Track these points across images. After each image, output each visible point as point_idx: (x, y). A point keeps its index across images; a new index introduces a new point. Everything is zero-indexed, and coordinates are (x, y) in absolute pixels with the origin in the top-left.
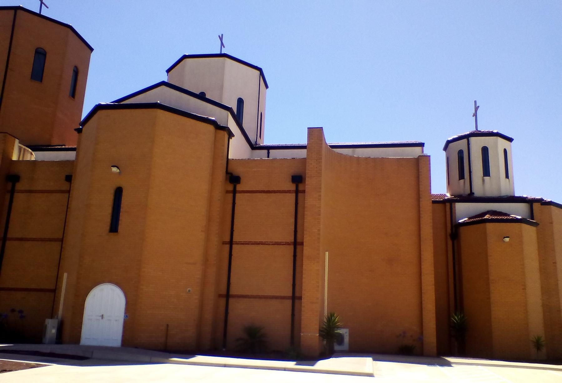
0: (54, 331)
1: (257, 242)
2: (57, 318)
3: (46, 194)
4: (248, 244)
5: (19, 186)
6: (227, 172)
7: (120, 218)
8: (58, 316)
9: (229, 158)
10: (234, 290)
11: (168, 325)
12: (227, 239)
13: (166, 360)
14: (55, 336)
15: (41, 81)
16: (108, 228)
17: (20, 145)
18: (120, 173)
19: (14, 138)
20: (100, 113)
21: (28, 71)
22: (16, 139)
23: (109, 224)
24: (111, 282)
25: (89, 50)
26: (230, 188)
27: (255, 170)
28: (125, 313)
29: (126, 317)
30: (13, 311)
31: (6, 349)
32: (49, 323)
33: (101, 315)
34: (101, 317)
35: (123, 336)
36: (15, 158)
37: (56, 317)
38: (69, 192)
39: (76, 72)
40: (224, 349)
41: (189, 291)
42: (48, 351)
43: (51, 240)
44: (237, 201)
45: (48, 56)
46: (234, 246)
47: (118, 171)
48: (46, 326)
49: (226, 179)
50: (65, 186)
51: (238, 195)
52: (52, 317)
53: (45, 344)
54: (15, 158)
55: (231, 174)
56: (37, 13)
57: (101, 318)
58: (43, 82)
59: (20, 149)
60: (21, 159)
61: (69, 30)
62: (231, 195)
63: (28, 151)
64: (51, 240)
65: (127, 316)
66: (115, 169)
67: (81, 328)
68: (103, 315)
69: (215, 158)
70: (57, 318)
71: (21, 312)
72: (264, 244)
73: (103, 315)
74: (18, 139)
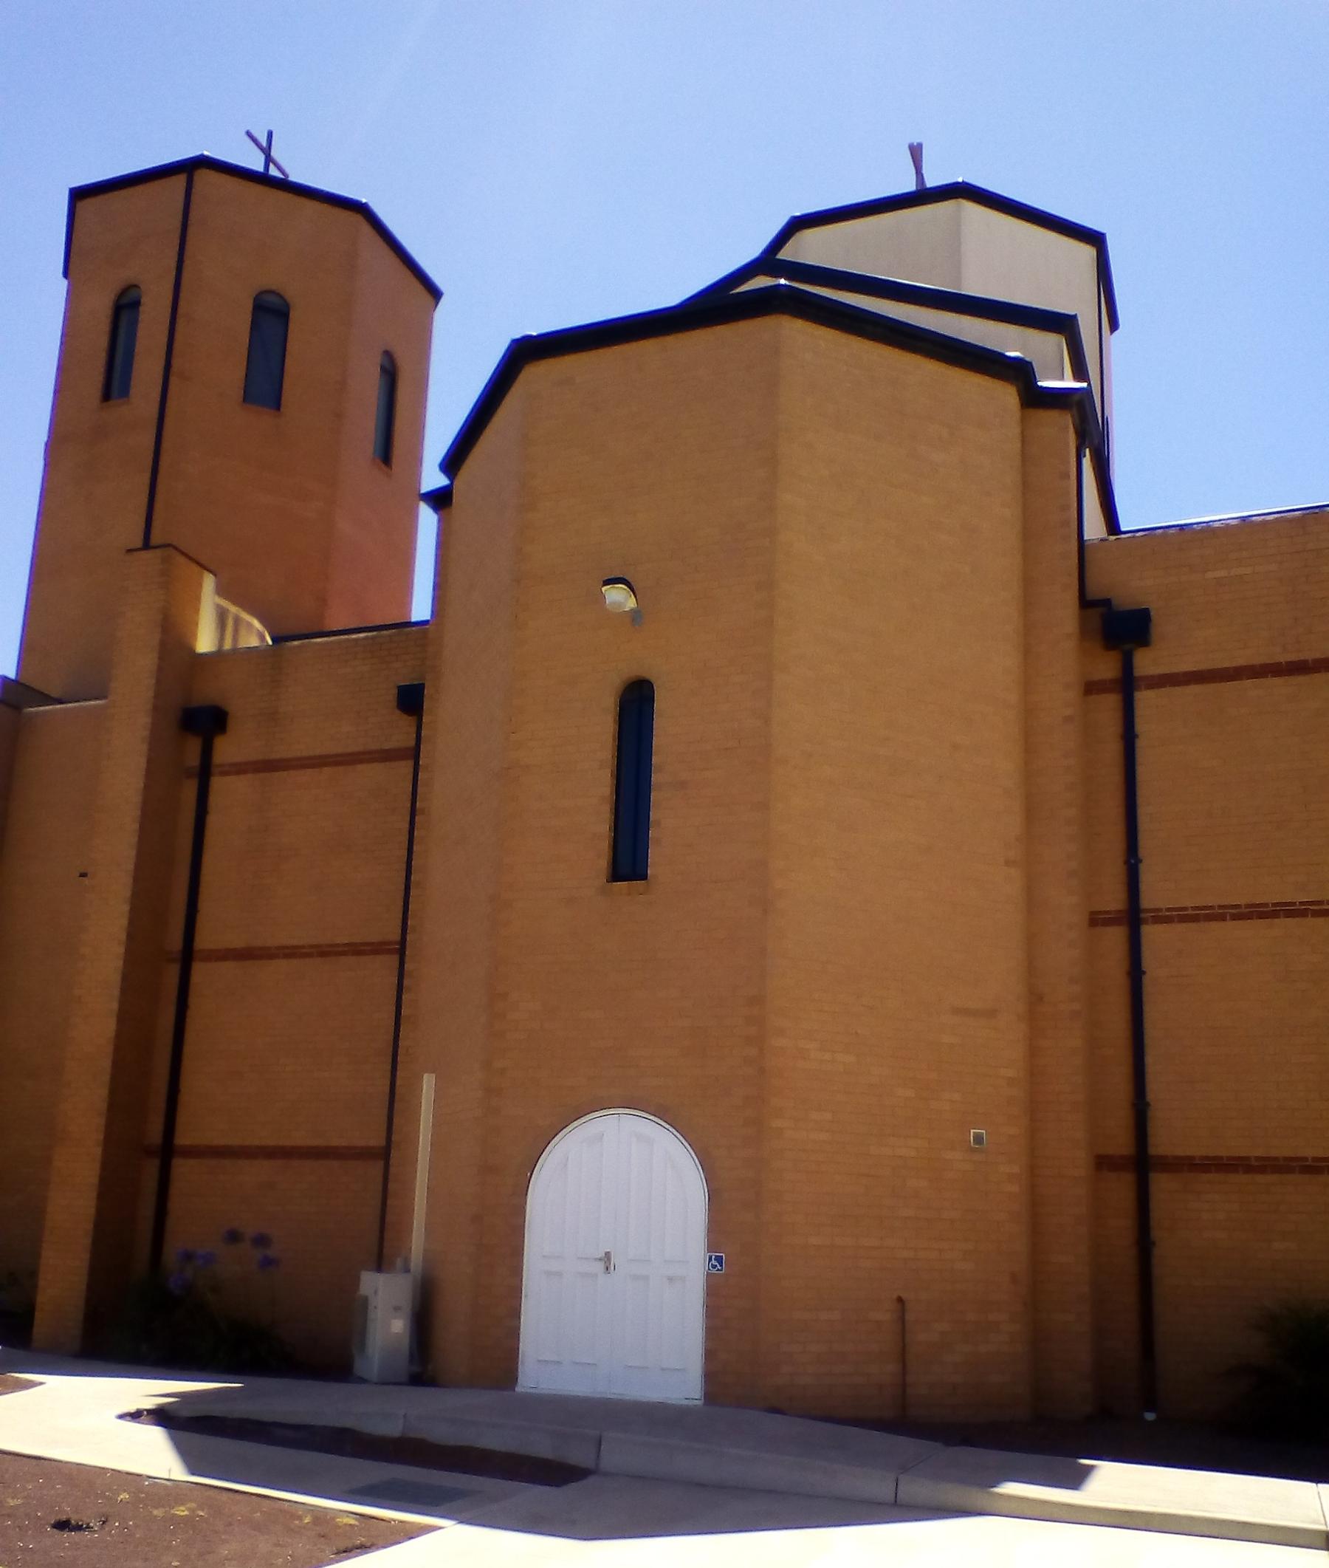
0: (399, 1326)
1: (1266, 905)
2: (407, 1270)
3: (327, 770)
4: (1222, 918)
5: (226, 750)
6: (1085, 602)
7: (653, 815)
8: (407, 1261)
9: (1085, 538)
10: (1163, 1142)
11: (900, 1300)
12: (1114, 900)
13: (974, 1496)
14: (405, 1343)
15: (278, 406)
16: (603, 863)
17: (225, 603)
18: (635, 616)
19: (196, 568)
20: (535, 375)
21: (233, 373)
22: (205, 571)
23: (605, 846)
24: (633, 1103)
25: (426, 297)
26: (1107, 667)
27: (1222, 573)
28: (712, 1245)
29: (714, 1262)
30: (233, 1237)
31: (218, 1410)
32: (376, 1292)
33: (602, 1254)
34: (601, 1266)
35: (710, 1355)
36: (205, 642)
37: (399, 1262)
38: (414, 754)
39: (390, 374)
40: (1150, 1416)
41: (978, 1139)
42: (390, 1428)
43: (356, 950)
44: (1141, 726)
45: (294, 316)
46: (1152, 934)
47: (631, 603)
48: (365, 1301)
49: (1084, 632)
50: (399, 732)
51: (1144, 699)
52: (380, 1263)
53: (362, 1380)
54: (205, 642)
55: (1106, 603)
56: (257, 173)
57: (600, 1267)
58: (282, 409)
59: (222, 616)
60: (228, 645)
61: (358, 219)
62: (1111, 702)
63: (250, 625)
64: (356, 950)
65: (719, 1259)
66: (617, 597)
67: (516, 1313)
68: (608, 1254)
69: (1030, 535)
70: (407, 1270)
71: (261, 1240)
72: (1302, 913)
73: (608, 1254)
74: (215, 575)
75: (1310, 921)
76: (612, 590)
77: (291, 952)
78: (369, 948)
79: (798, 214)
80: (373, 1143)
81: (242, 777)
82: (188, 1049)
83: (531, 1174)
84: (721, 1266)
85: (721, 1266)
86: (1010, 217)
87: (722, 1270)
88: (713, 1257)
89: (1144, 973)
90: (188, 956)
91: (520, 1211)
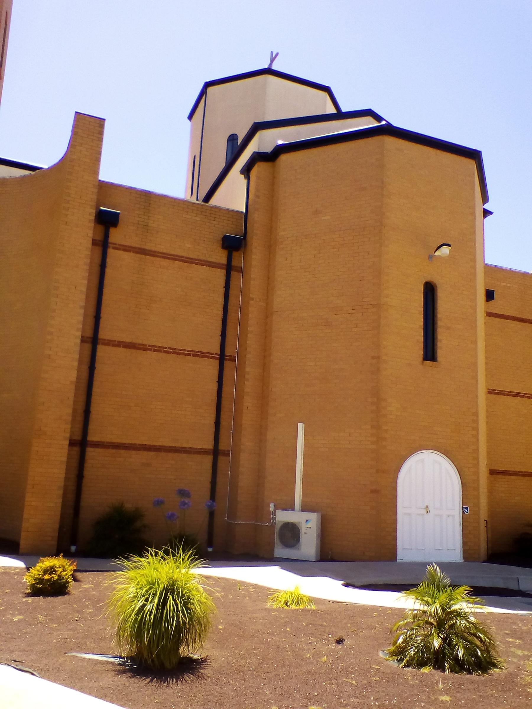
33: (425, 507)
57: (424, 511)
68: (427, 507)
72: (522, 397)
73: (427, 507)
75: (524, 399)
76: (447, 248)
77: (159, 350)
78: (142, 346)
79: (208, 81)
80: (205, 447)
81: (127, 253)
82: (96, 390)
83: (461, 478)
84: (468, 511)
85: (468, 511)
86: (200, 105)
87: (467, 513)
88: (465, 508)
89: (217, 382)
90: (222, 357)
91: (395, 488)
